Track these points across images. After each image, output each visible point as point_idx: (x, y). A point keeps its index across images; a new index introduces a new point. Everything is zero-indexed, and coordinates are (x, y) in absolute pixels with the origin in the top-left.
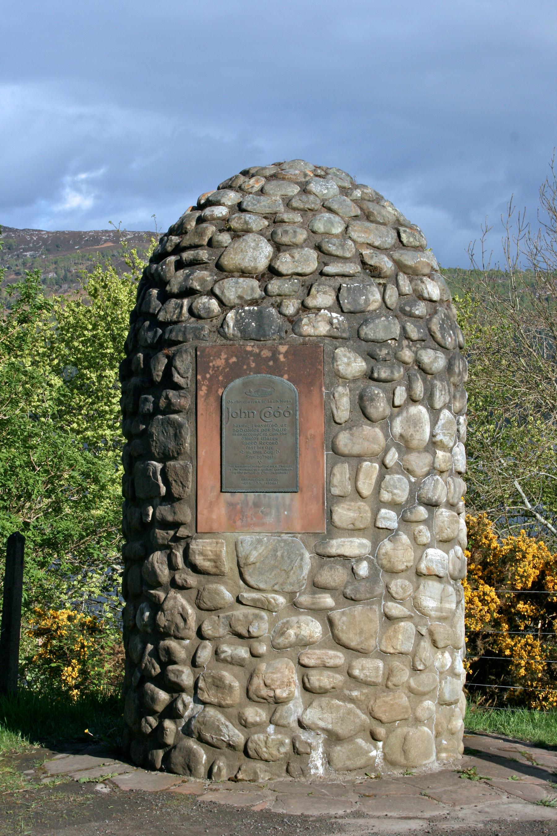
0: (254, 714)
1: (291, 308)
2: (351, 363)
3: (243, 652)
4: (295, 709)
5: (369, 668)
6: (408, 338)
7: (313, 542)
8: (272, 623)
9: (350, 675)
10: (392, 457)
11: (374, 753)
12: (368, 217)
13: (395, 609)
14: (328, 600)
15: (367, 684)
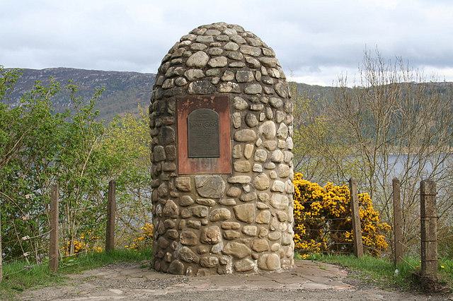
0: (204, 249)
1: (215, 80)
2: (241, 103)
3: (198, 223)
4: (220, 246)
5: (250, 229)
6: (266, 93)
7: (226, 177)
8: (210, 211)
9: (243, 233)
10: (259, 142)
11: (253, 265)
12: (249, 44)
13: (262, 205)
14: (233, 201)
15: (250, 236)
